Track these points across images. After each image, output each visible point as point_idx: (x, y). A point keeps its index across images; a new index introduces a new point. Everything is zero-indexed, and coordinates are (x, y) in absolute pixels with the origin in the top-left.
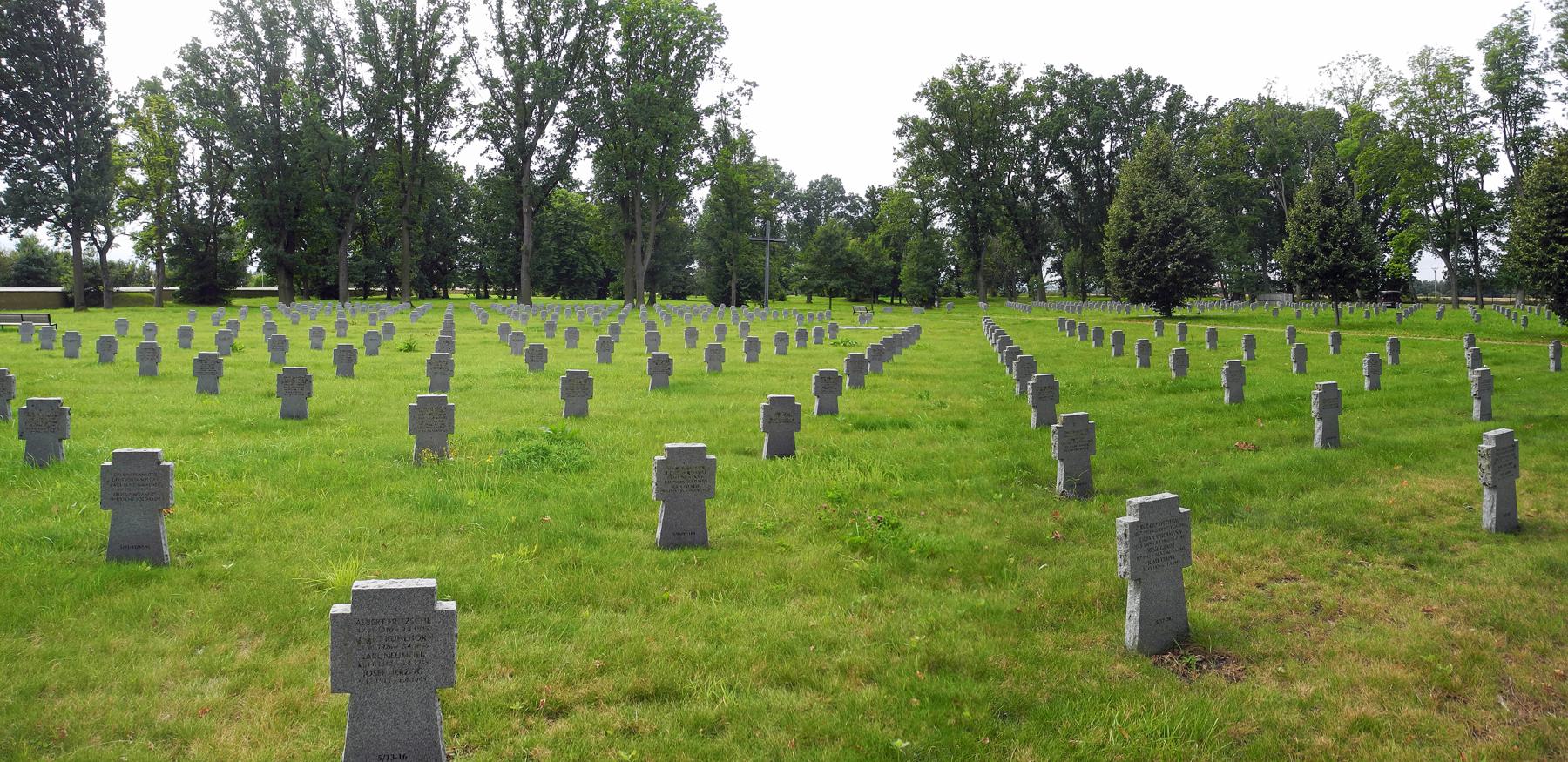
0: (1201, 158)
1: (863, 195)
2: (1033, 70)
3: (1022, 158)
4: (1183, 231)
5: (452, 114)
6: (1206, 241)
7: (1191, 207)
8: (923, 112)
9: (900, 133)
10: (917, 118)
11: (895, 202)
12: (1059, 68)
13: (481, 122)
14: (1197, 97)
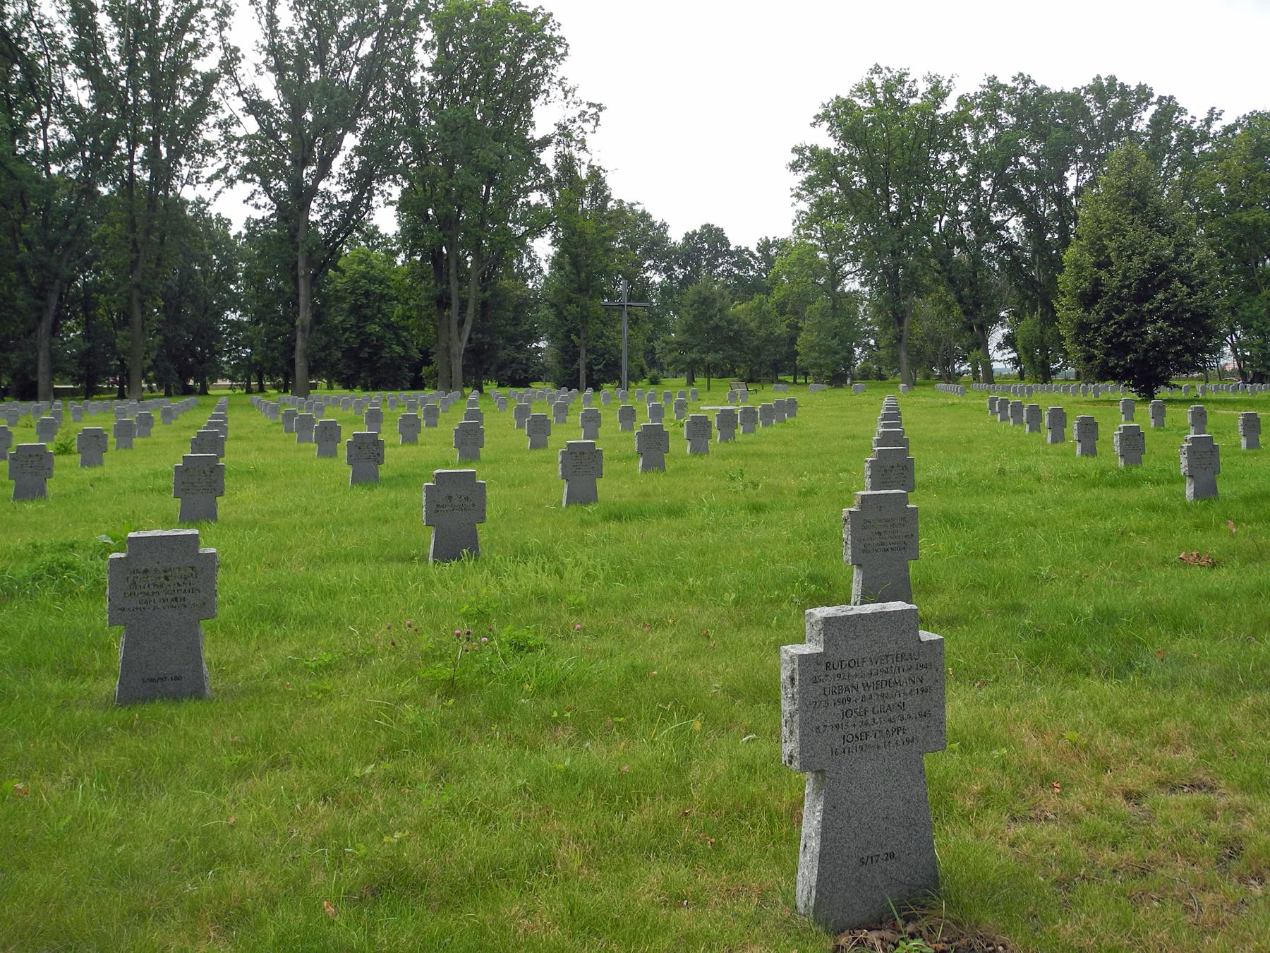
0: (1203, 195)
1: (753, 248)
2: (968, 84)
3: (957, 199)
4: (1168, 281)
5: (208, 149)
6: (1200, 294)
7: (1178, 251)
8: (825, 140)
9: (795, 167)
10: (817, 147)
11: (794, 256)
12: (1005, 79)
13: (246, 160)
14: (1194, 110)
